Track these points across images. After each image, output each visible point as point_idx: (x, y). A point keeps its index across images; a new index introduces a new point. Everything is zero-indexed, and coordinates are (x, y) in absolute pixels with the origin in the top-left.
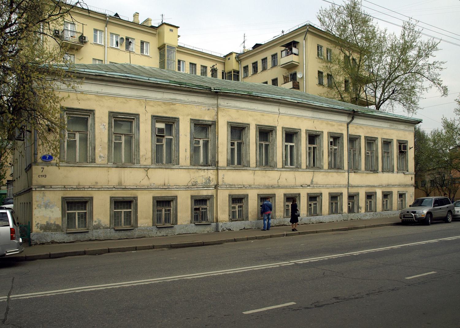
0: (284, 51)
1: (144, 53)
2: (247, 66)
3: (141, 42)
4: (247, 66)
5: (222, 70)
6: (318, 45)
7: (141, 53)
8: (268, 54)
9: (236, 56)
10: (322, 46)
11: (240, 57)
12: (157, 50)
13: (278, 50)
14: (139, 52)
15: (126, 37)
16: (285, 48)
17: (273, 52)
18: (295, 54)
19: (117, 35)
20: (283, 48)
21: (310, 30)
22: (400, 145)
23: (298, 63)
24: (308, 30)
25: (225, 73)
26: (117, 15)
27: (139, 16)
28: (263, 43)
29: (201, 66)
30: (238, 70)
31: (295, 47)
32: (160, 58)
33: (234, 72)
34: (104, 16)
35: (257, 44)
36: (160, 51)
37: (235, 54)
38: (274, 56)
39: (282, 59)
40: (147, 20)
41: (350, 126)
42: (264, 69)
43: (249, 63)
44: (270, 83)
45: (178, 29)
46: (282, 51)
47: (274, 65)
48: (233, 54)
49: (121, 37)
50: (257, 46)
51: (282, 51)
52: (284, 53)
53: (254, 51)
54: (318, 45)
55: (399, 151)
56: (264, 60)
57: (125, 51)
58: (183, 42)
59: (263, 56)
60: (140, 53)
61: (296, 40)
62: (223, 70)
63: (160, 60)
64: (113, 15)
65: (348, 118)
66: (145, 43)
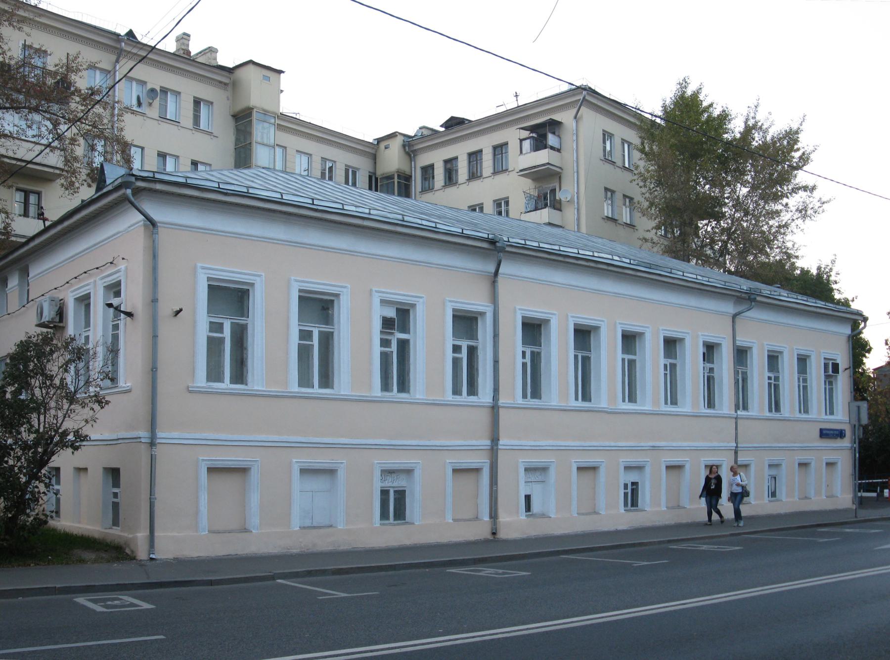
0: (528, 141)
1: (200, 127)
2: (432, 166)
3: (194, 101)
4: (432, 166)
5: (369, 172)
6: (603, 130)
7: (194, 125)
8: (486, 143)
9: (404, 141)
10: (613, 135)
11: (413, 145)
12: (231, 123)
13: (512, 136)
14: (187, 121)
15: (161, 87)
16: (529, 132)
17: (497, 138)
18: (552, 148)
19: (143, 83)
20: (526, 134)
21: (588, 98)
22: (827, 362)
23: (560, 168)
24: (584, 98)
25: (376, 179)
26: (130, 34)
27: (190, 42)
28: (473, 119)
29: (322, 158)
30: (408, 172)
31: (554, 133)
32: (237, 140)
33: (399, 176)
34: (115, 37)
35: (452, 118)
36: (236, 122)
37: (402, 138)
38: (500, 149)
39: (522, 157)
40: (211, 51)
41: (737, 319)
42: (474, 175)
43: (436, 158)
44: (489, 208)
45: (282, 74)
46: (521, 141)
47: (499, 169)
48: (397, 135)
49: (149, 86)
50: (454, 123)
51: (521, 141)
52: (527, 145)
53: (448, 135)
54: (603, 130)
55: (825, 375)
56: (475, 157)
57: (192, 128)
58: (288, 105)
59: (472, 145)
60: (191, 126)
61: (557, 117)
62: (371, 171)
63: (236, 145)
64: (123, 32)
65: (144, 229)
66: (202, 103)
